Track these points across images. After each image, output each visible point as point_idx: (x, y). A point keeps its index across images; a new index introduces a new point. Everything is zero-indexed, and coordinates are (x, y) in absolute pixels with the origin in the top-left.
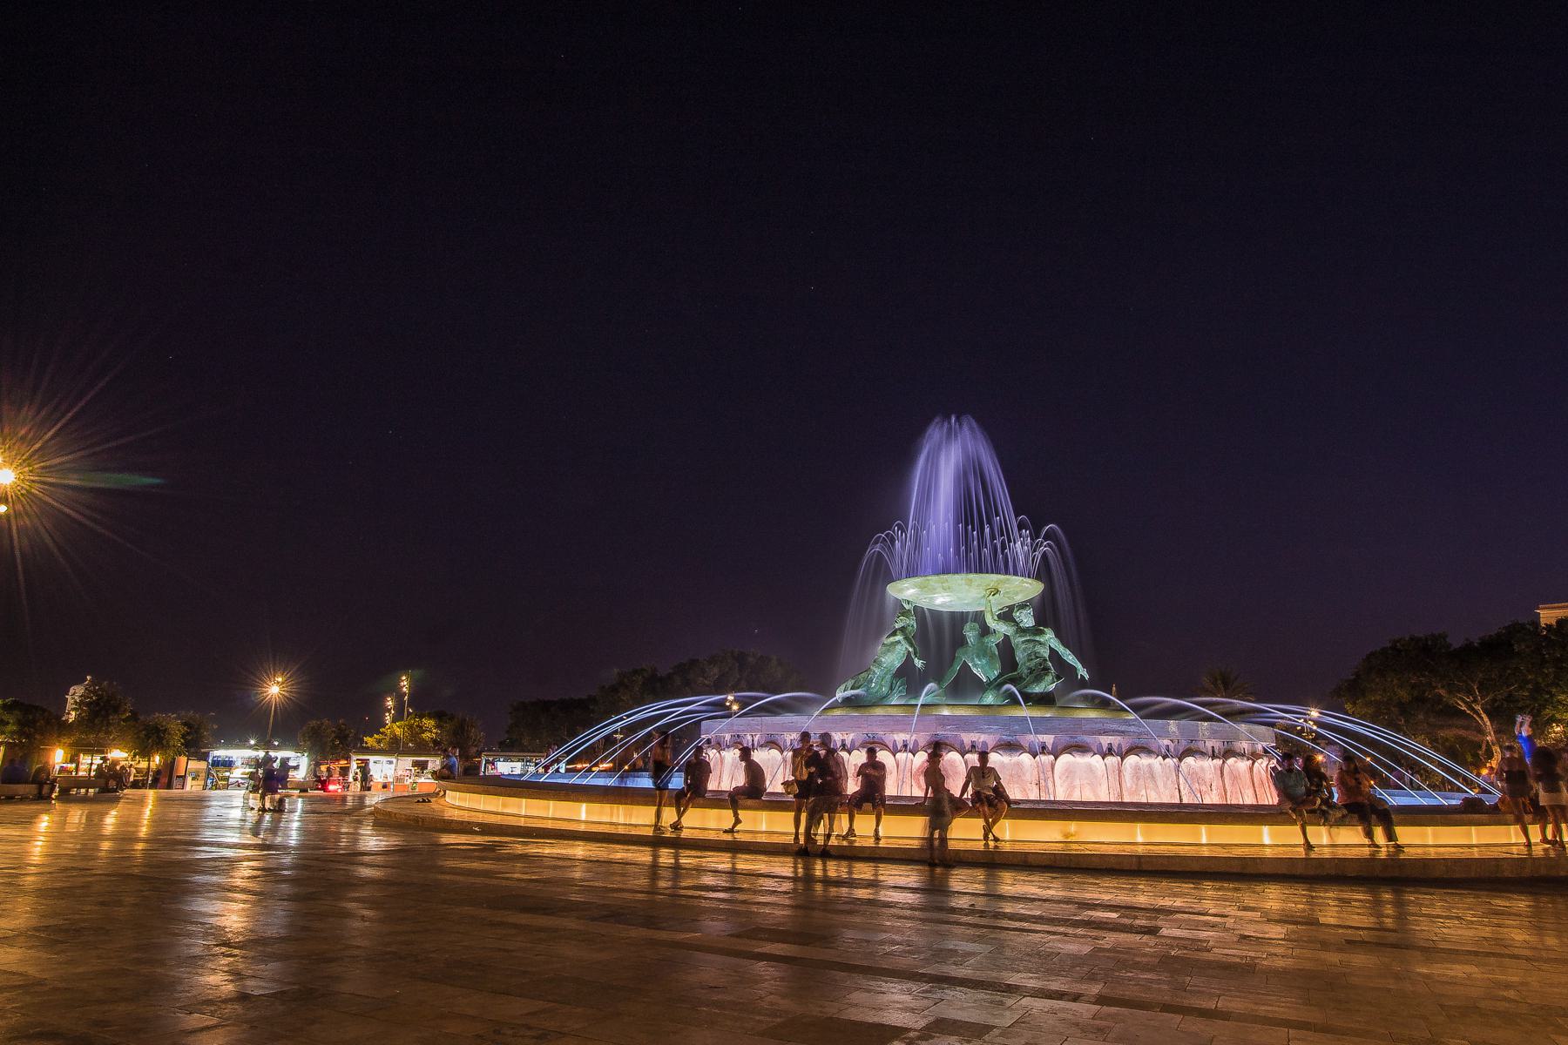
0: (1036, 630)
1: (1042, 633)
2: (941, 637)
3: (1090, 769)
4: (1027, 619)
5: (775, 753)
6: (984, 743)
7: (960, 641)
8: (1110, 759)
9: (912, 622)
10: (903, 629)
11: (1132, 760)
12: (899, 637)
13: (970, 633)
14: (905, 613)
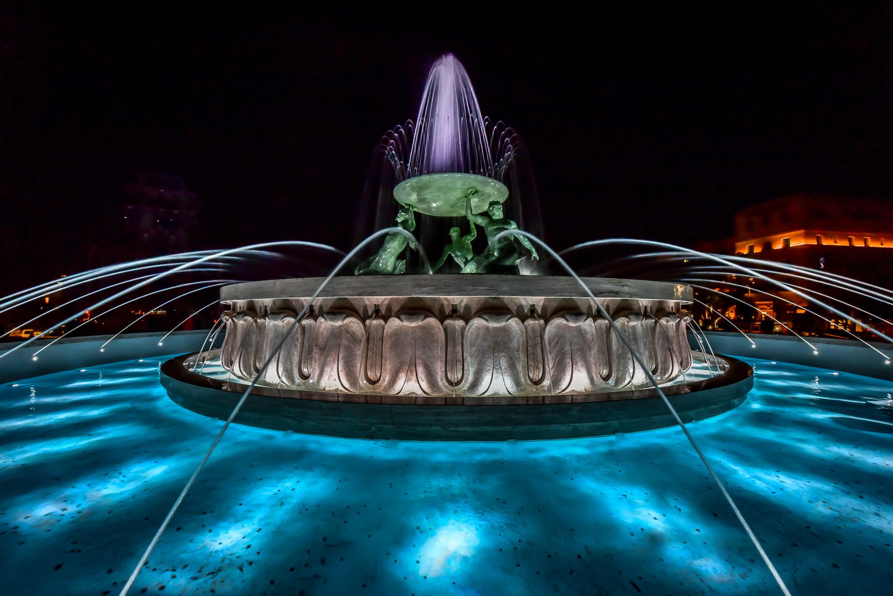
0: (505, 221)
1: (509, 224)
2: (435, 238)
3: (580, 332)
4: (498, 214)
5: (250, 319)
6: (467, 307)
7: (449, 240)
8: (530, 322)
9: (410, 217)
10: (404, 224)
11: (620, 322)
12: (400, 228)
13: (454, 233)
14: (406, 211)
